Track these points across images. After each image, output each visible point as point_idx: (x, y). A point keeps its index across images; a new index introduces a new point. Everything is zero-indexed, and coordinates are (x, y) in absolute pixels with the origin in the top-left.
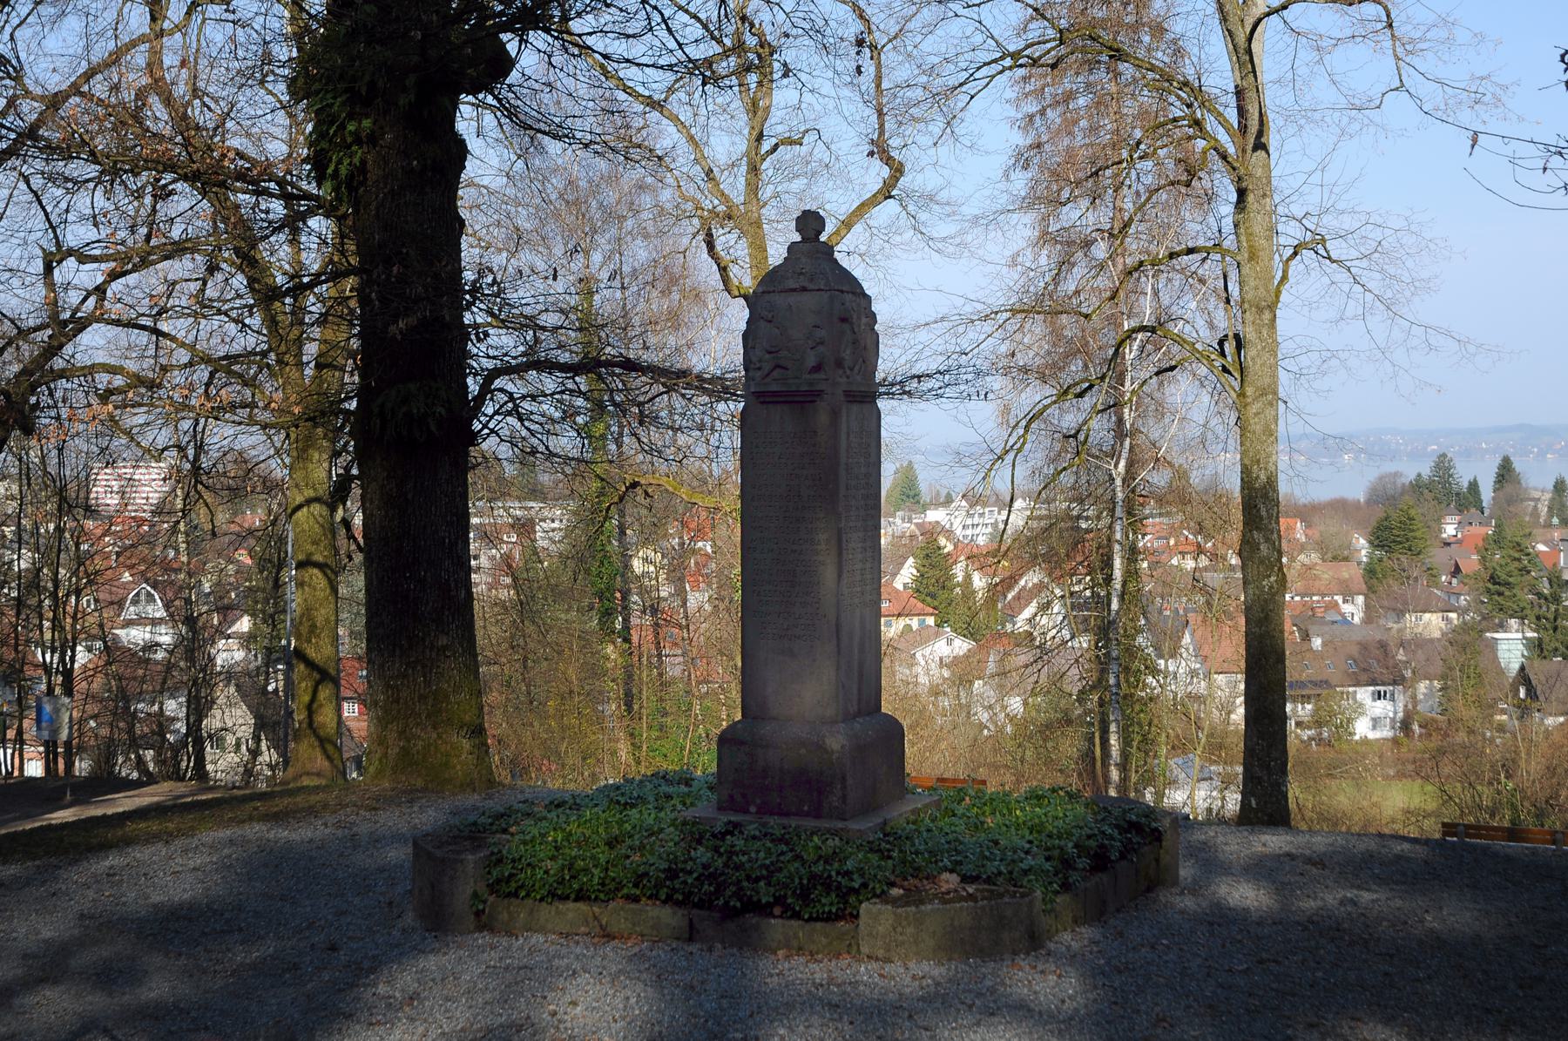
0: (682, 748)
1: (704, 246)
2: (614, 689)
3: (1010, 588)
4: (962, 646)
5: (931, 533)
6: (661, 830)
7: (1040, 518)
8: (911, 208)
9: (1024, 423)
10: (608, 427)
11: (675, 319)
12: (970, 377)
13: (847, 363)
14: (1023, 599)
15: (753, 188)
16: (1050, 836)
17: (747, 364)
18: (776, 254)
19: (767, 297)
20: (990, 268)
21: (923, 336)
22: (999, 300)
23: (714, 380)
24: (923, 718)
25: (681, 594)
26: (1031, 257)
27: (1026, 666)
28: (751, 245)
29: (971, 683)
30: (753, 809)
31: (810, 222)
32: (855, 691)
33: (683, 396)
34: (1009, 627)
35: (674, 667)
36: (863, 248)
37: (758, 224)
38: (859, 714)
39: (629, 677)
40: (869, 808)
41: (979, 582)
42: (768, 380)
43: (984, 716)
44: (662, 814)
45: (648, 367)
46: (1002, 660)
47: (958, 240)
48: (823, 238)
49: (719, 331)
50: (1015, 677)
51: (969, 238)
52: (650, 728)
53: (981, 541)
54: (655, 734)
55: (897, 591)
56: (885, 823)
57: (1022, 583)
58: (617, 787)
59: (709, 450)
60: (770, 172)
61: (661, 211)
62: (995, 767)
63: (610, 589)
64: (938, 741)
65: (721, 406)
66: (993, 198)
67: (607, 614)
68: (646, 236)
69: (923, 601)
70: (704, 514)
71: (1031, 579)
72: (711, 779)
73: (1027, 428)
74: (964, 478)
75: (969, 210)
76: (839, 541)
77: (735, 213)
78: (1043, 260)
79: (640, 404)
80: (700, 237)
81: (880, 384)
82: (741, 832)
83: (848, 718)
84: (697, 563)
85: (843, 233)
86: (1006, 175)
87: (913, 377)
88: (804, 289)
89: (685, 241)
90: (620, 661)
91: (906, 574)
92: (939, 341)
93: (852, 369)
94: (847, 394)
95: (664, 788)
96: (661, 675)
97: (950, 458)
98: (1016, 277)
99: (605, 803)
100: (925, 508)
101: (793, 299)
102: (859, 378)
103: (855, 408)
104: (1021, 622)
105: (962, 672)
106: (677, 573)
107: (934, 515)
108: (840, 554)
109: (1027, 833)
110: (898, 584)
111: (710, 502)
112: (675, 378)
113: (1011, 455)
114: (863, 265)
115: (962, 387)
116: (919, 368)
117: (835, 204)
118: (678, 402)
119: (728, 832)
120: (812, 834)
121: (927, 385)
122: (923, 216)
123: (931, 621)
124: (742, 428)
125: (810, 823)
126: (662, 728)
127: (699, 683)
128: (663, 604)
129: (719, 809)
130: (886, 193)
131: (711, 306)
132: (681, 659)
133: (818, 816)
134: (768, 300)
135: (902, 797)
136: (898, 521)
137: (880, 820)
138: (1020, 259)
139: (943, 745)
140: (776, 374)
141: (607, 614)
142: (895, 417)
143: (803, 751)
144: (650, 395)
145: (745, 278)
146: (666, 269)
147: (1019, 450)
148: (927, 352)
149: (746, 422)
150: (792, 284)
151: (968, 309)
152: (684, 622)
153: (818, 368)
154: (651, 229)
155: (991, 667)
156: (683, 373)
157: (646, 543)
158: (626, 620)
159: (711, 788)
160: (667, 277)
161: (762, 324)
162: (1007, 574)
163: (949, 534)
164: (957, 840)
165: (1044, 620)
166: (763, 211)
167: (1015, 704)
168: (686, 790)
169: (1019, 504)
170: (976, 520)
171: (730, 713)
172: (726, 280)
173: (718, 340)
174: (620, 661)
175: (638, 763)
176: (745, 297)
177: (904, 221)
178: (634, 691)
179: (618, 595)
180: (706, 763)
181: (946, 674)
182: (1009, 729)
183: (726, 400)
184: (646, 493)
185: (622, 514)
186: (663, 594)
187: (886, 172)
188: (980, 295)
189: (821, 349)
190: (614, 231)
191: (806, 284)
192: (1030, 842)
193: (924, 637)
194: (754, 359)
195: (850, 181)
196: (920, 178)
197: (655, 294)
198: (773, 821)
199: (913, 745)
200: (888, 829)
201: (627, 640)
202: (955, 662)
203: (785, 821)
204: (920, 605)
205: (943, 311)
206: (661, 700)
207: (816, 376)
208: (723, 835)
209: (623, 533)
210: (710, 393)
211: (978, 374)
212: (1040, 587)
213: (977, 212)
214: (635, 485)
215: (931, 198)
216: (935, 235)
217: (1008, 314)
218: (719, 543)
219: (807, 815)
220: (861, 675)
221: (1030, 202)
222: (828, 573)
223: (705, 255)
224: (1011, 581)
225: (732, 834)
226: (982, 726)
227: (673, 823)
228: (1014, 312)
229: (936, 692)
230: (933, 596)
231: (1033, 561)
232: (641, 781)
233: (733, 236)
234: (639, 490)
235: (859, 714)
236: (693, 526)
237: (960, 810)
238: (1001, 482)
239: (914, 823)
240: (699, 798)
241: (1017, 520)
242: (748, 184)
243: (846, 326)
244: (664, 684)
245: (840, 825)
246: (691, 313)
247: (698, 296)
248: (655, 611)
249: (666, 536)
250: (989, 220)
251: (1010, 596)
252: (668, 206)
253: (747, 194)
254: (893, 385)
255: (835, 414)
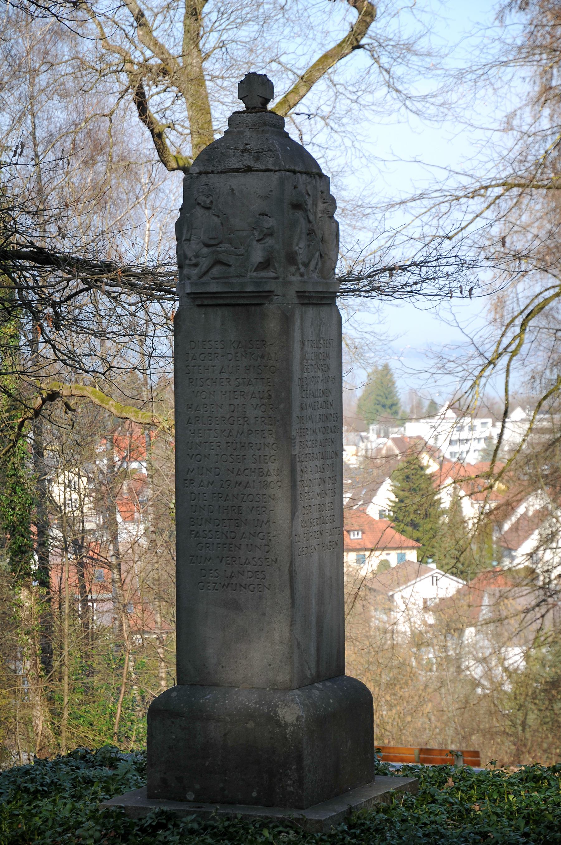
0: (112, 715)
1: (134, 107)
2: (29, 644)
3: (506, 516)
4: (449, 586)
5: (412, 451)
6: (79, 825)
7: (542, 431)
8: (384, 60)
9: (519, 321)
10: (20, 327)
11: (100, 197)
12: (450, 269)
13: (301, 258)
14: (522, 530)
15: (193, 37)
16: (550, 827)
17: (182, 259)
18: (220, 124)
19: (204, 178)
20: (479, 134)
21: (396, 219)
22: (491, 170)
23: (146, 273)
24: (402, 674)
25: (111, 526)
26: (529, 119)
27: (527, 611)
28: (191, 106)
29: (461, 631)
30: (190, 796)
31: (255, 88)
32: (313, 650)
33: (108, 294)
34: (506, 563)
35: (102, 615)
36: (326, 110)
37: (199, 80)
38: (318, 678)
39: (47, 629)
40: (333, 791)
41: (470, 510)
42: (204, 279)
43: (477, 671)
44: (80, 805)
45: (65, 259)
46: (497, 604)
47: (439, 100)
48: (271, 106)
49: (153, 209)
50: (514, 623)
51: (453, 97)
52: (73, 690)
53: (473, 459)
54: (78, 697)
55: (371, 521)
56: (350, 811)
57: (521, 510)
58: (26, 772)
59: (140, 352)
60: (214, 16)
61: (81, 64)
62: (490, 734)
63: (24, 522)
64: (421, 704)
65: (154, 307)
66: (482, 49)
67: (20, 552)
68: (65, 94)
69: (403, 532)
70: (138, 431)
71: (533, 504)
72: (140, 758)
73: (523, 326)
74: (446, 388)
75: (455, 63)
76: (293, 470)
77: (172, 67)
78: (545, 124)
79: (54, 305)
80: (130, 96)
81: (341, 280)
82: (176, 825)
83: (305, 684)
84: (130, 489)
85: (302, 90)
86: (500, 16)
87: (385, 270)
88: (249, 169)
89: (112, 100)
90: (36, 608)
91: (384, 497)
92: (418, 222)
93: (306, 265)
94: (301, 295)
95: (84, 772)
96: (86, 625)
97: (432, 362)
98: (510, 143)
99: (11, 791)
100: (405, 420)
101: (237, 181)
102: (315, 276)
103: (311, 312)
104: (520, 558)
105: (450, 618)
106: (106, 502)
107: (414, 429)
108: (293, 486)
109: (522, 823)
110: (373, 511)
111: (144, 416)
112: (97, 272)
113: (505, 360)
114: (326, 130)
115: (442, 282)
116: (396, 256)
117: (286, 56)
118: (105, 302)
119: (162, 826)
120: (263, 826)
121: (401, 278)
122: (398, 70)
123: (412, 556)
124: (176, 332)
125: (260, 813)
126: (87, 689)
127: (132, 633)
128: (90, 538)
129: (149, 797)
130: (353, 41)
131: (144, 179)
132: (110, 605)
133: (270, 805)
134: (209, 175)
135: (370, 780)
136: (372, 435)
137: (345, 808)
138: (516, 122)
139: (428, 707)
140: (216, 271)
141: (20, 552)
142: (360, 319)
143: (251, 725)
144: (67, 293)
145: (184, 145)
146: (89, 134)
147: (514, 353)
148: (400, 238)
149: (179, 325)
150: (234, 163)
151: (452, 184)
152: (114, 561)
153: (265, 265)
154: (70, 85)
155: (485, 613)
156: (108, 267)
157: (68, 465)
158: (43, 559)
159: (140, 770)
160: (92, 144)
161: (199, 212)
162: (502, 501)
163: (433, 451)
164: (437, 832)
165: (548, 555)
166: (206, 65)
167: (515, 656)
168: (110, 773)
169: (517, 414)
170: (465, 434)
171: (164, 679)
172: (161, 148)
173: (148, 228)
174: (36, 608)
175: (58, 733)
176: (185, 170)
177: (376, 76)
178: (54, 645)
179: (34, 529)
180: (135, 743)
181: (431, 619)
182: (508, 687)
183: (160, 299)
184: (67, 406)
185: (38, 431)
186: (88, 526)
187: (353, 16)
188: (467, 166)
189: (270, 241)
190: (24, 87)
191: (251, 163)
192: (526, 835)
193: (404, 575)
194: (190, 254)
195: (310, 27)
196: (394, 22)
197: (76, 164)
198: (214, 810)
199: (391, 707)
200: (354, 819)
201: (44, 583)
202: (441, 607)
203: (229, 811)
204: (398, 536)
205: (422, 186)
206: (87, 656)
207: (263, 274)
208: (155, 828)
209: (39, 452)
210: (140, 290)
211: (462, 264)
212: (543, 515)
213: (462, 65)
214: (53, 396)
215: (409, 48)
216: (413, 92)
217: (498, 191)
218: (156, 465)
219: (256, 802)
220: (320, 633)
221: (528, 51)
222: (280, 510)
223: (136, 118)
224: (508, 507)
225: (164, 827)
226: (475, 684)
227: (93, 816)
228: (507, 185)
229: (419, 641)
230: (415, 525)
231: (534, 484)
232: (56, 763)
233: (169, 96)
234: (58, 402)
235: (318, 678)
236: (126, 443)
237: (440, 797)
238: (493, 388)
239: (385, 811)
240: (125, 782)
241: (515, 433)
242: (187, 31)
243: (299, 214)
244: (89, 636)
245: (296, 814)
246: (119, 186)
247: (127, 167)
248: (78, 546)
249: (92, 457)
250: (479, 75)
251: (507, 526)
252: (90, 58)
253: (186, 44)
254: (358, 279)
255: (286, 320)
